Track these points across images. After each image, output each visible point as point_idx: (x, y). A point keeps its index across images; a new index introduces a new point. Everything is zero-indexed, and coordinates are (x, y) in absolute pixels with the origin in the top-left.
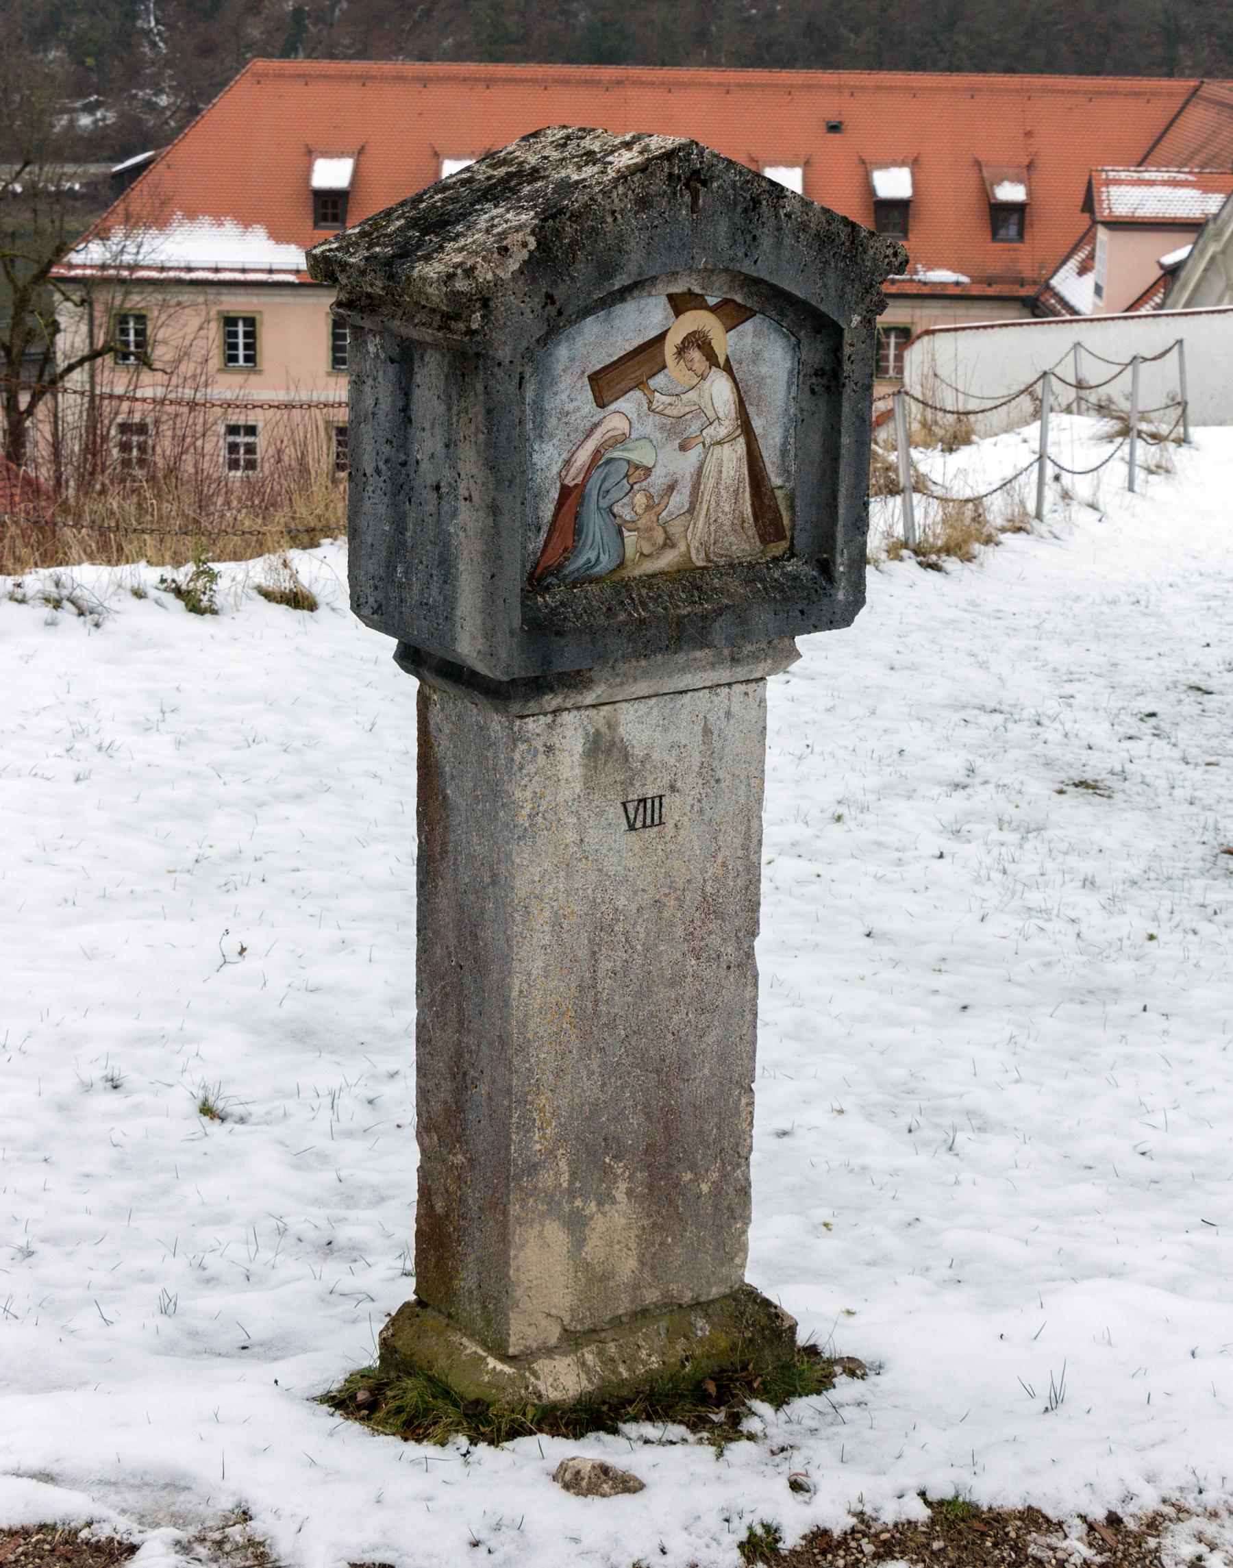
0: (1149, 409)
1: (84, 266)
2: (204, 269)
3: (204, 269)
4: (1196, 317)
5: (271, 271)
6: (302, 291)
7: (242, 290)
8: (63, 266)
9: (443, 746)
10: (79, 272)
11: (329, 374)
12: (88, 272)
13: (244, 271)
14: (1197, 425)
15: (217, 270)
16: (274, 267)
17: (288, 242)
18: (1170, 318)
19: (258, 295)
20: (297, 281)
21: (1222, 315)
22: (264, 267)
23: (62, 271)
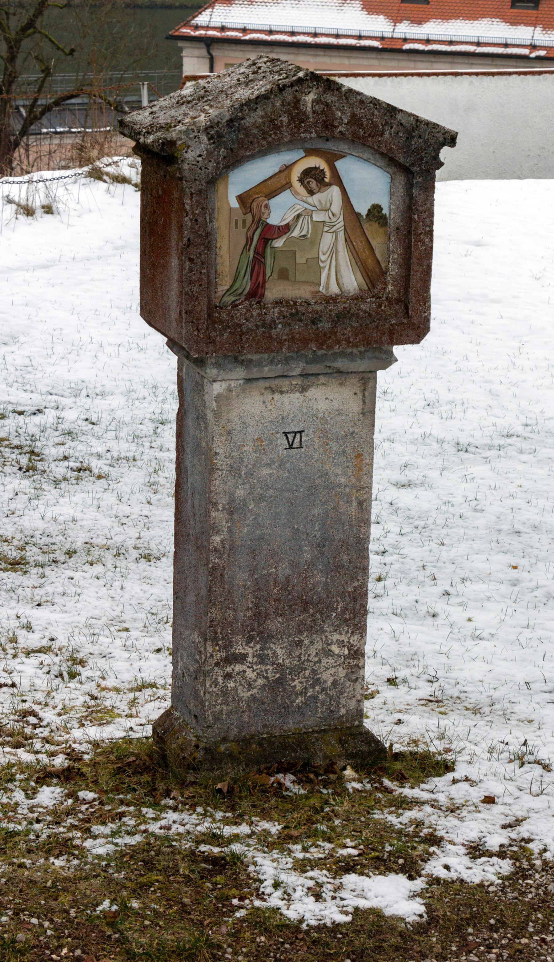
0: (305, 159)
1: (208, 28)
2: (304, 34)
3: (304, 34)
4: (504, 77)
5: (360, 37)
6: (386, 56)
7: (335, 53)
8: (190, 26)
9: (188, 462)
10: (202, 32)
11: (457, 133)
12: (211, 33)
13: (337, 36)
14: (442, 180)
15: (315, 35)
16: (482, 40)
17: (378, 13)
18: (474, 78)
19: (349, 57)
20: (380, 47)
21: (537, 77)
22: (354, 33)
23: (189, 31)
